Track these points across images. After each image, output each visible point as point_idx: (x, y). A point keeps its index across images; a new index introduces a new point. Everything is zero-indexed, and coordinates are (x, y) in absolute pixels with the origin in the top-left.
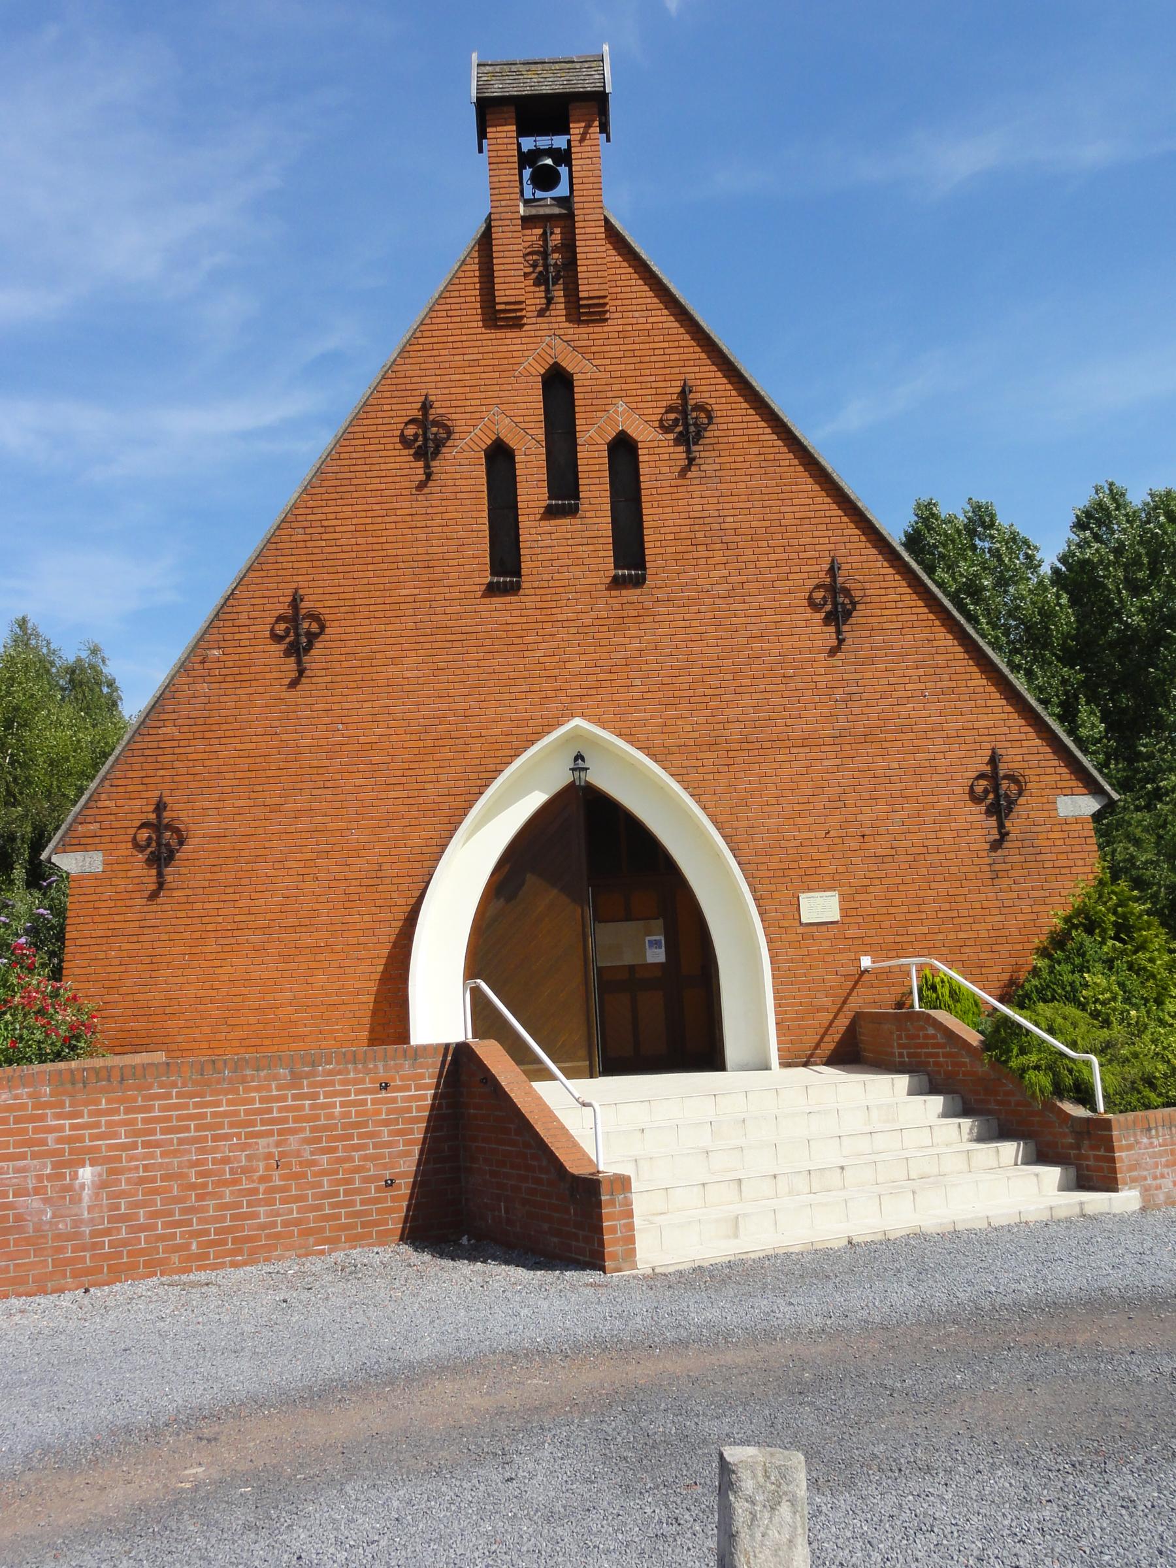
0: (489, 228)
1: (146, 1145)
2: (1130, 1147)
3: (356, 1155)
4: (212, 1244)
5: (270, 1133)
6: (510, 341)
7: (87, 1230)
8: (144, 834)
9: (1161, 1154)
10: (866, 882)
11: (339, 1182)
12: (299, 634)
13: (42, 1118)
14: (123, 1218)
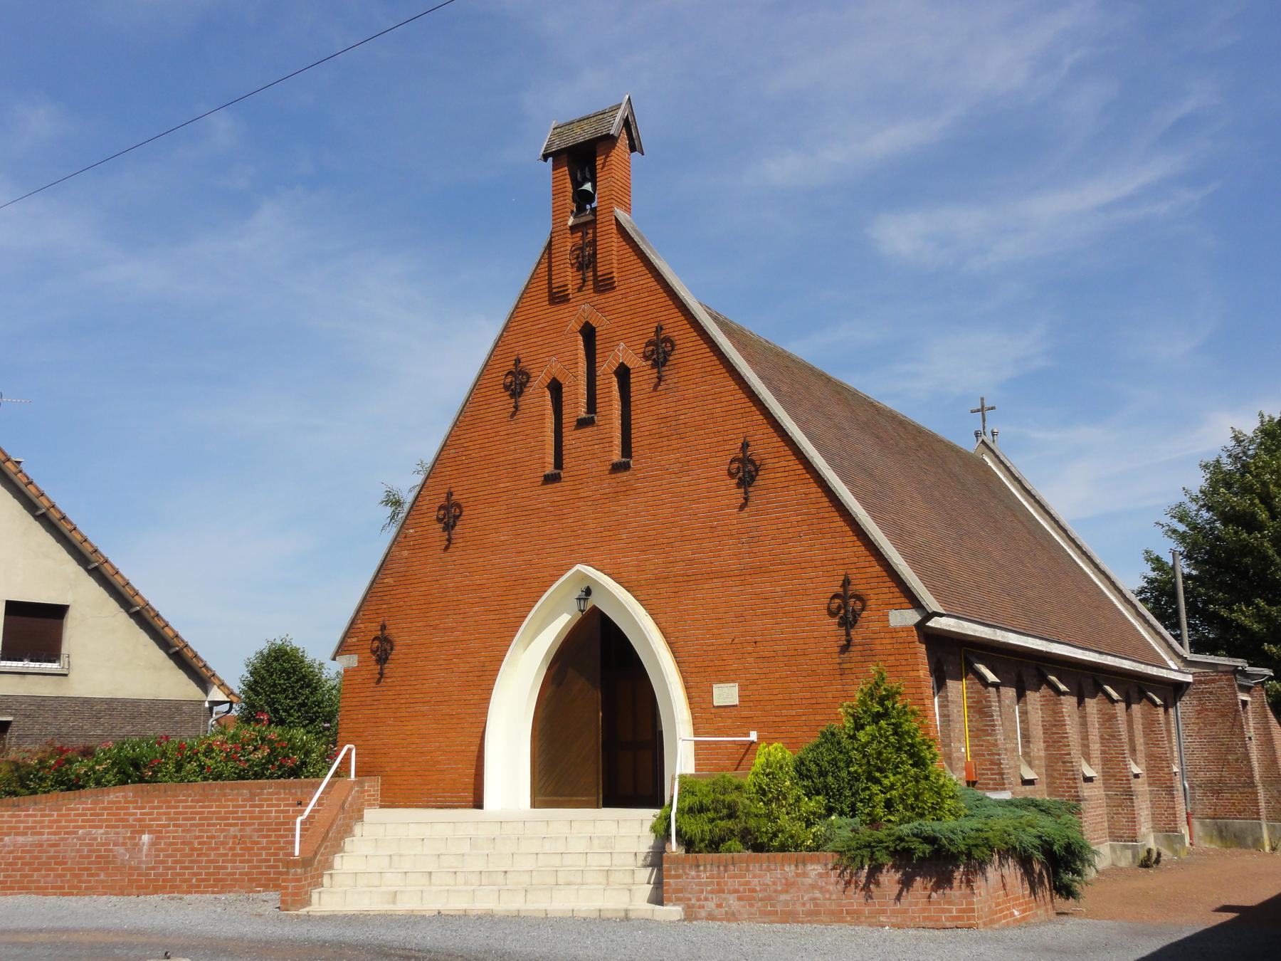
0: (550, 242)
1: (175, 825)
2: (677, 877)
3: (282, 840)
4: (203, 880)
5: (236, 825)
6: (563, 311)
7: (144, 866)
8: (376, 644)
9: (707, 884)
10: (756, 676)
11: (271, 855)
12: (450, 515)
13: (127, 808)
14: (161, 862)
